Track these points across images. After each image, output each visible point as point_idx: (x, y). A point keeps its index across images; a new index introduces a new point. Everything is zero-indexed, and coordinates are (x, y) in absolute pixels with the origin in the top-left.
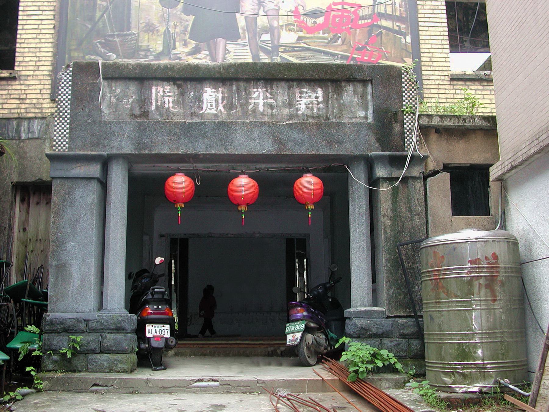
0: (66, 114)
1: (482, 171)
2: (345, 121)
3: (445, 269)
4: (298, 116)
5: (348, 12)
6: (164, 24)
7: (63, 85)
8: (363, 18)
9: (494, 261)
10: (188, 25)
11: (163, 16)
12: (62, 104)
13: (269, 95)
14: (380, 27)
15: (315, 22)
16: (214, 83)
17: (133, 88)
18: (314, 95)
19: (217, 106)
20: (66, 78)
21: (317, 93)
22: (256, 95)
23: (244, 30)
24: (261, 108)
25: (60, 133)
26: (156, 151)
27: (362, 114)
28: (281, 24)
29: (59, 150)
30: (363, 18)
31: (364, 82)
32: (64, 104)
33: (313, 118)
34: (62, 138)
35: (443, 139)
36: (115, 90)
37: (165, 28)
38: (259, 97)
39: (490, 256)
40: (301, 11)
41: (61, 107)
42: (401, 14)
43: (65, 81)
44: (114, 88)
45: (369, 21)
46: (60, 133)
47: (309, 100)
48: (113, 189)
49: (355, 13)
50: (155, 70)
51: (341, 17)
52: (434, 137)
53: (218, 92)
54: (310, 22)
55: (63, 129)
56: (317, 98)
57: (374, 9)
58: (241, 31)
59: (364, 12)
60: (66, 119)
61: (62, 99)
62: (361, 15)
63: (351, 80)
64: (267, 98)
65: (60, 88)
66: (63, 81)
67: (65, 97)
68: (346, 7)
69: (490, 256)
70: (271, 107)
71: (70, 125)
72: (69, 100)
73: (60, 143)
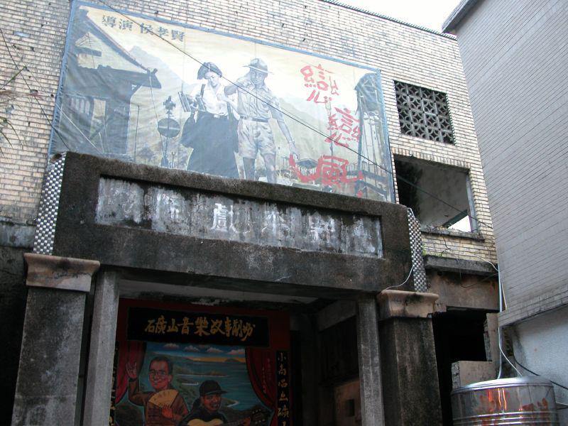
0: (53, 210)
1: (476, 319)
2: (357, 255)
3: (496, 416)
4: (311, 245)
5: (336, 165)
6: (162, 152)
7: (52, 176)
8: (349, 173)
9: (545, 407)
10: (187, 157)
11: (161, 144)
12: (49, 198)
13: (283, 220)
14: (365, 184)
15: (308, 172)
16: (225, 199)
17: (134, 193)
18: (327, 225)
19: (228, 224)
20: (56, 169)
21: (330, 223)
22: (269, 217)
23: (242, 170)
24: (274, 231)
25: (44, 232)
26: (160, 267)
27: (373, 249)
28: (277, 169)
29: (41, 253)
30: (349, 173)
31: (374, 218)
32: (52, 198)
33: (327, 249)
34: (46, 239)
35: (444, 282)
36: (114, 191)
37: (162, 156)
38: (272, 219)
39: (541, 402)
40: (296, 160)
41: (48, 201)
42: (382, 174)
43: (55, 171)
44: (112, 189)
45: (356, 177)
46: (44, 232)
47: (320, 230)
48: (103, 308)
49: (343, 167)
50: (163, 175)
51: (332, 170)
52: (437, 279)
53: (229, 209)
54: (304, 171)
55: (47, 227)
56: (329, 228)
57: (359, 166)
58: (239, 171)
59: (351, 168)
60: (53, 216)
61: (50, 192)
62: (348, 170)
63: (361, 214)
64: (280, 222)
65: (49, 178)
66: (53, 171)
67: (53, 190)
68: (336, 162)
69: (541, 402)
70: (285, 233)
71: (64, 174)
72: (53, 228)
73: (42, 244)
